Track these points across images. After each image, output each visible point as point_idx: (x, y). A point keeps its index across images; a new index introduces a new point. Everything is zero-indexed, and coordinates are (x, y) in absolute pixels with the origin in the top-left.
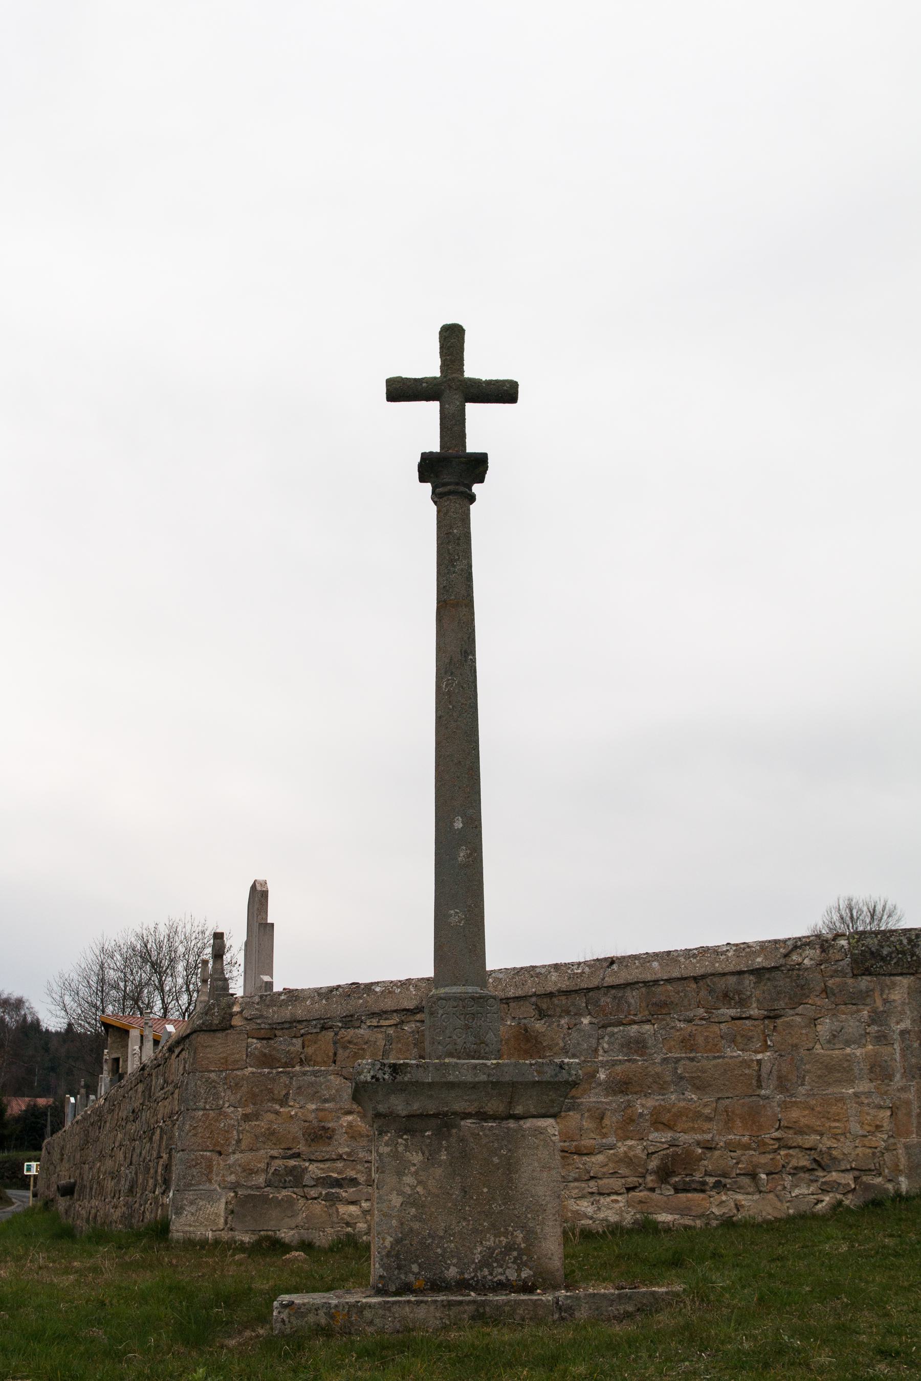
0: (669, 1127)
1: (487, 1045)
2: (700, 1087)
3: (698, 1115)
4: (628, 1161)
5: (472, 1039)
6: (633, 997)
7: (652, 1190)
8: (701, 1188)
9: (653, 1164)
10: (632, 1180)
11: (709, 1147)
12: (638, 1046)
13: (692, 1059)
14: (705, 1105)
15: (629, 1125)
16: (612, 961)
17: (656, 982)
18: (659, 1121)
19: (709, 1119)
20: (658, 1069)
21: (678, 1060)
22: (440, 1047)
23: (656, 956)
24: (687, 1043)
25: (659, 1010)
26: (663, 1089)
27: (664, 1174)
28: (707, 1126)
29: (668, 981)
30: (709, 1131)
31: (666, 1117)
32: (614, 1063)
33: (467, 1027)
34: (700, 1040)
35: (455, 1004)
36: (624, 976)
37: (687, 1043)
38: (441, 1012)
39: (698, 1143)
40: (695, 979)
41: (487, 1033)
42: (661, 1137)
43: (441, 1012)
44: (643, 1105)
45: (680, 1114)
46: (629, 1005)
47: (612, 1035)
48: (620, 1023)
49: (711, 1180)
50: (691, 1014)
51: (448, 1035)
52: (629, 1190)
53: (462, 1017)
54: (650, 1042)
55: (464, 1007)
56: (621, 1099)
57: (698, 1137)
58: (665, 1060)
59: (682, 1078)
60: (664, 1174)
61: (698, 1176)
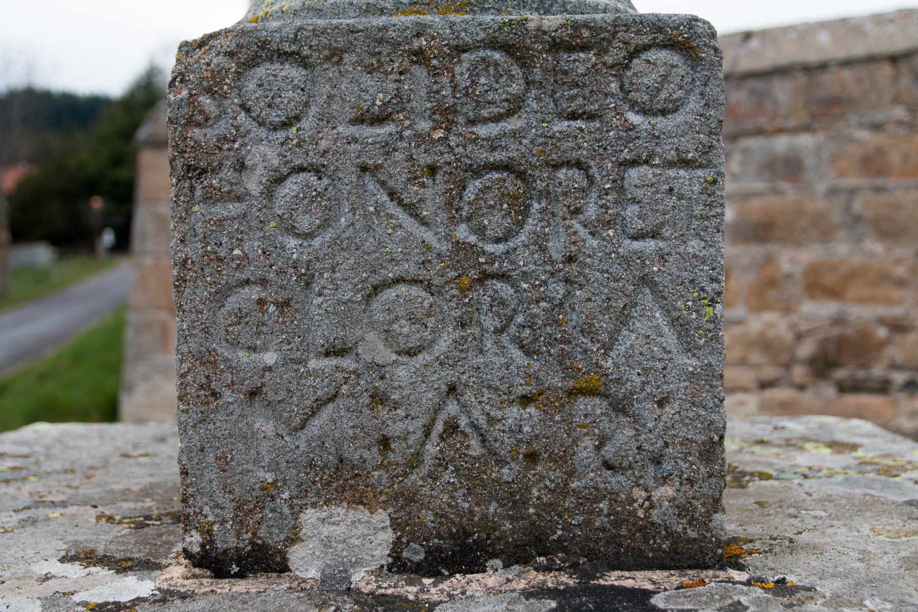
0: (833, 293)
1: (620, 407)
2: (889, 231)
3: (884, 277)
4: (765, 344)
5: (503, 360)
6: (782, 90)
7: (801, 388)
8: (883, 387)
9: (806, 349)
10: (770, 372)
11: (898, 327)
12: (790, 168)
13: (878, 190)
14: (898, 261)
15: (768, 290)
16: (747, 36)
17: (823, 66)
18: (817, 285)
19: (901, 283)
20: (820, 204)
21: (853, 192)
22: (265, 426)
23: (823, 25)
24: (873, 164)
25: (826, 110)
26: (826, 234)
27: (822, 366)
28: (896, 294)
29: (847, 63)
30: (900, 302)
31: (829, 280)
32: (747, 196)
33: (475, 272)
34: (895, 159)
35: (376, 91)
36: (769, 58)
37: (873, 164)
38: (264, 154)
39: (882, 321)
40: (894, 59)
41: (624, 319)
42: (818, 311)
43: (264, 154)
44: (793, 260)
45: (855, 274)
46: (776, 102)
47: (746, 151)
48: (759, 132)
49: (899, 378)
50: (879, 117)
51: (320, 337)
52: (764, 385)
53: (432, 195)
54: (810, 161)
55: (445, 115)
56: (757, 251)
57: (883, 311)
58: (833, 192)
59: (858, 219)
60: (822, 366)
61: (878, 371)
